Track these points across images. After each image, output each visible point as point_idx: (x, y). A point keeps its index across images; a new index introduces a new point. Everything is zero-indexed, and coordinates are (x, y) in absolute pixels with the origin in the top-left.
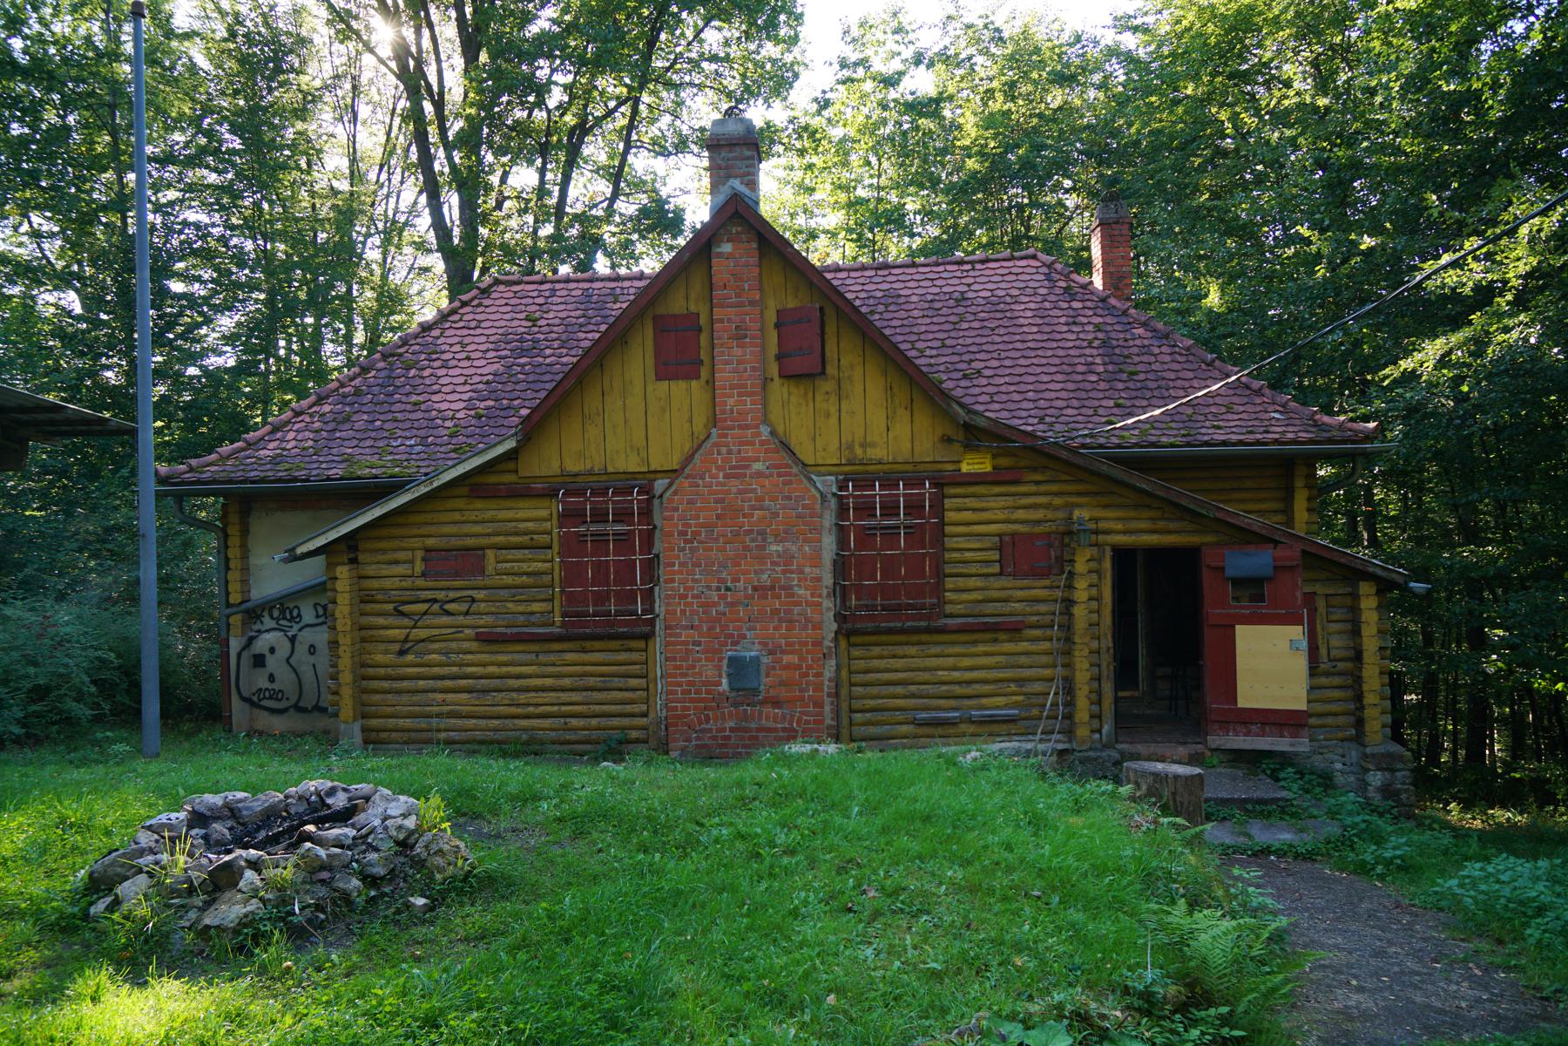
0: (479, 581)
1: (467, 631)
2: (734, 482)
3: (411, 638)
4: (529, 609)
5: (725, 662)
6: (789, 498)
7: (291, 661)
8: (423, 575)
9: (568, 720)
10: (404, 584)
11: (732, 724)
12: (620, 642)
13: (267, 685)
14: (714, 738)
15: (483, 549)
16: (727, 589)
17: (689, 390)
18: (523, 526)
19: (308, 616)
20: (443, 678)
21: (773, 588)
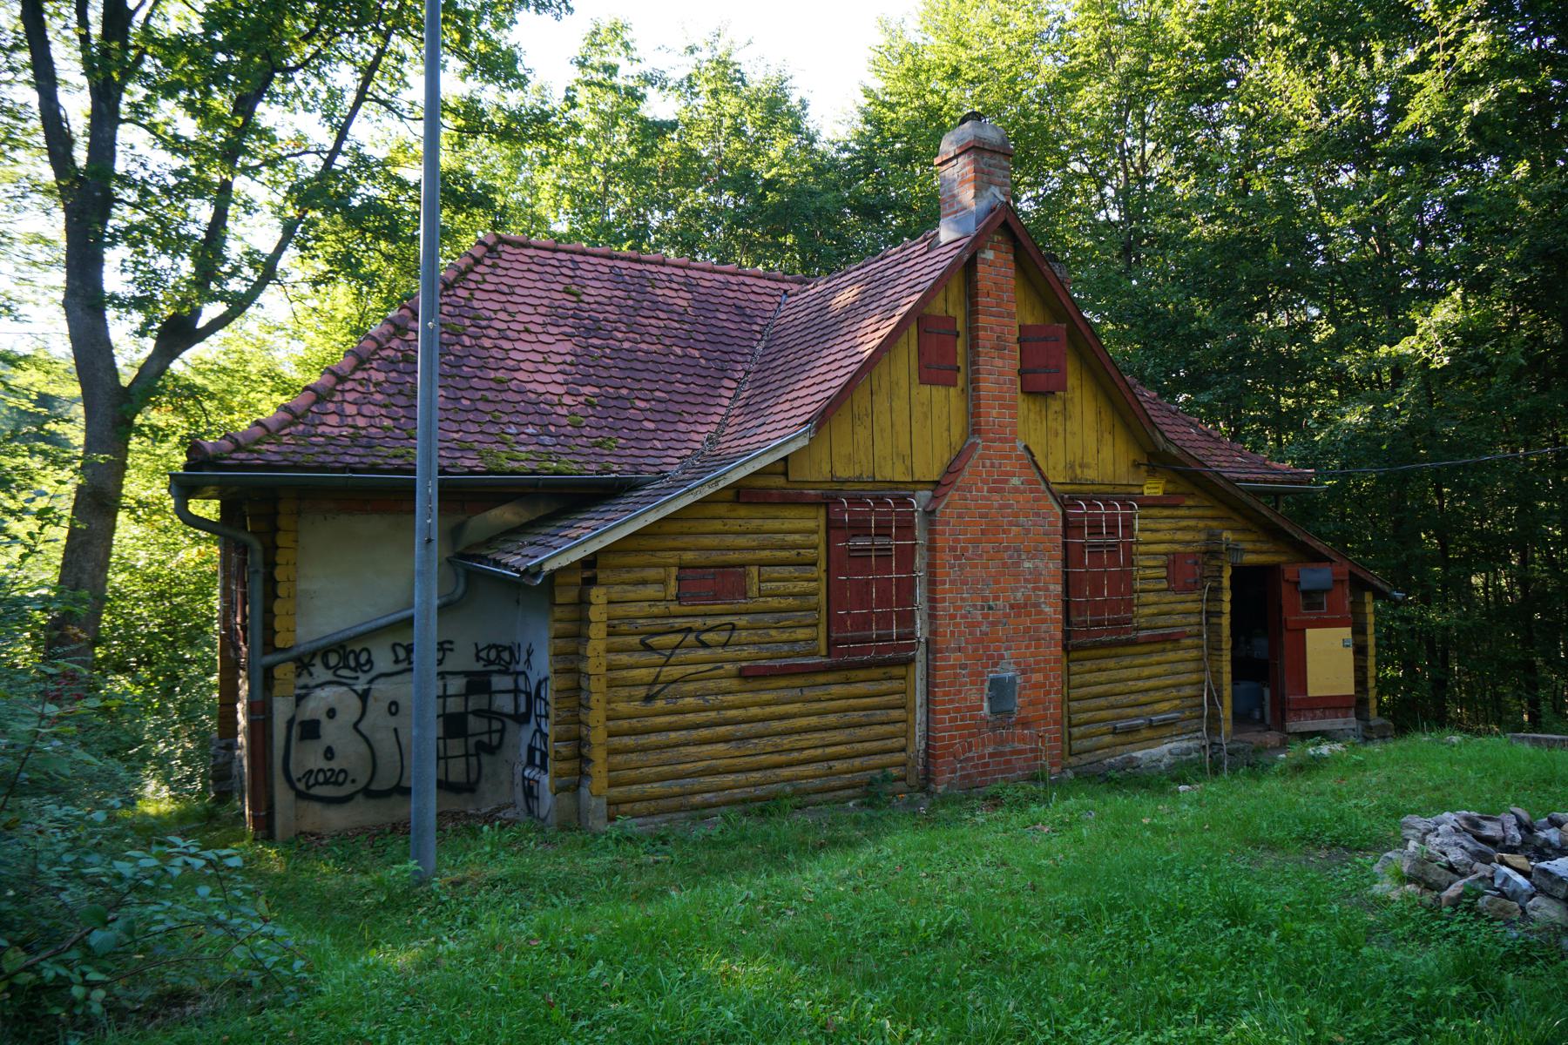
0: (742, 604)
1: (728, 666)
2: (996, 496)
3: (661, 678)
4: (794, 636)
5: (987, 685)
6: (1038, 515)
7: (362, 726)
8: (678, 598)
9: (831, 763)
10: (655, 610)
11: (990, 750)
12: (883, 670)
13: (322, 764)
14: (975, 766)
15: (743, 566)
16: (990, 608)
17: (947, 397)
18: (790, 538)
19: (383, 660)
20: (697, 726)
21: (1026, 606)
